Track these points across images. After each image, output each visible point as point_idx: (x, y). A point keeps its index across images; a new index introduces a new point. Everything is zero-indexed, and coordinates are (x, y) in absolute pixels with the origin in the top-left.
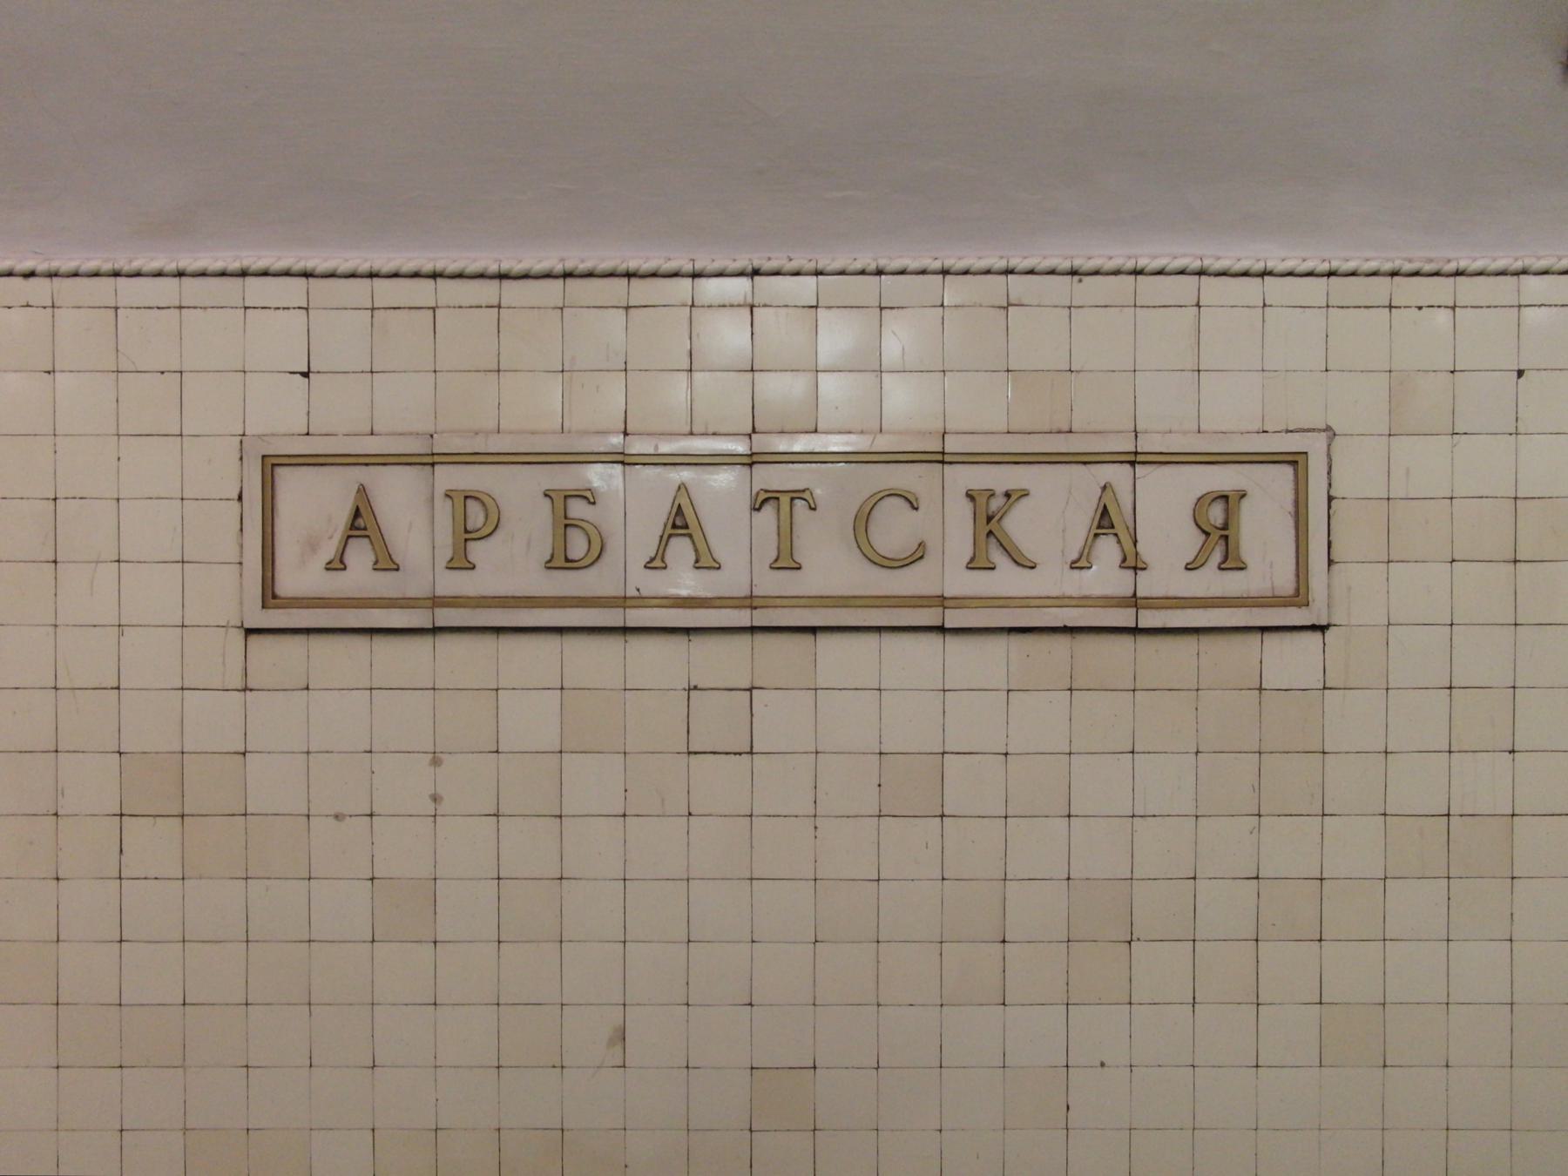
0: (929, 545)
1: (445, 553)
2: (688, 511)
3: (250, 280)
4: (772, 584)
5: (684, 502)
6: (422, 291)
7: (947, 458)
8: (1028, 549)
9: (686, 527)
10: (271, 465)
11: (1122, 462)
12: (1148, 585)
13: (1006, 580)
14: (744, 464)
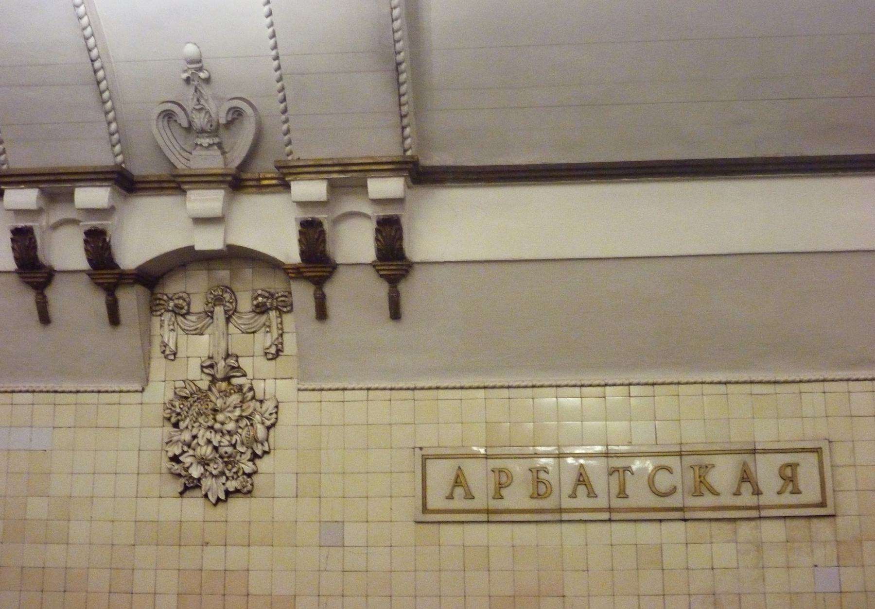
0: (678, 487)
1: (492, 492)
2: (462, 478)
3: (324, 392)
4: (617, 503)
5: (582, 471)
6: (316, 395)
7: (609, 455)
8: (717, 487)
9: (584, 481)
10: (425, 459)
11: (601, 457)
12: (764, 500)
13: (708, 500)
14: (604, 457)
